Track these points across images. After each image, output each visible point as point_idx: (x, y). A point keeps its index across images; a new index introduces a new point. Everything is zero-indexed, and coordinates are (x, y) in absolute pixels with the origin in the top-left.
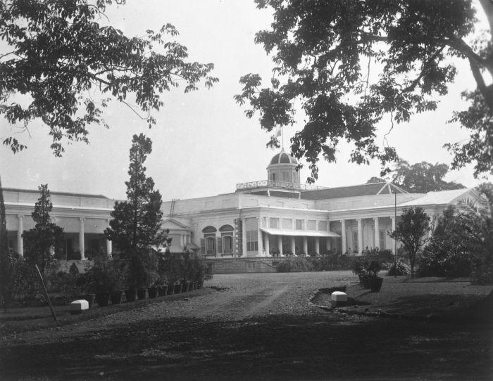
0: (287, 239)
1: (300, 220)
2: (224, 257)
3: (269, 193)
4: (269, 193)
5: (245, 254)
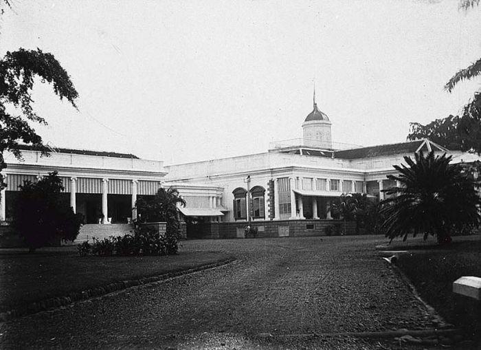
0: (321, 200)
1: (336, 180)
2: (255, 220)
3: (301, 151)
4: (301, 151)
5: (252, 220)
